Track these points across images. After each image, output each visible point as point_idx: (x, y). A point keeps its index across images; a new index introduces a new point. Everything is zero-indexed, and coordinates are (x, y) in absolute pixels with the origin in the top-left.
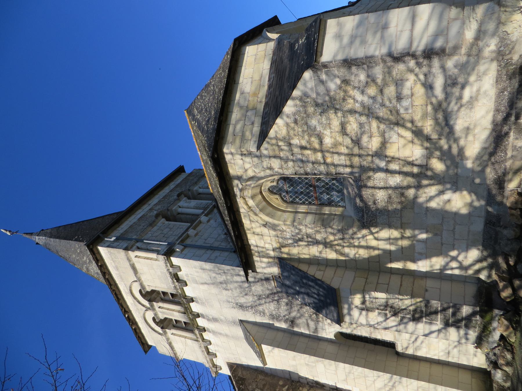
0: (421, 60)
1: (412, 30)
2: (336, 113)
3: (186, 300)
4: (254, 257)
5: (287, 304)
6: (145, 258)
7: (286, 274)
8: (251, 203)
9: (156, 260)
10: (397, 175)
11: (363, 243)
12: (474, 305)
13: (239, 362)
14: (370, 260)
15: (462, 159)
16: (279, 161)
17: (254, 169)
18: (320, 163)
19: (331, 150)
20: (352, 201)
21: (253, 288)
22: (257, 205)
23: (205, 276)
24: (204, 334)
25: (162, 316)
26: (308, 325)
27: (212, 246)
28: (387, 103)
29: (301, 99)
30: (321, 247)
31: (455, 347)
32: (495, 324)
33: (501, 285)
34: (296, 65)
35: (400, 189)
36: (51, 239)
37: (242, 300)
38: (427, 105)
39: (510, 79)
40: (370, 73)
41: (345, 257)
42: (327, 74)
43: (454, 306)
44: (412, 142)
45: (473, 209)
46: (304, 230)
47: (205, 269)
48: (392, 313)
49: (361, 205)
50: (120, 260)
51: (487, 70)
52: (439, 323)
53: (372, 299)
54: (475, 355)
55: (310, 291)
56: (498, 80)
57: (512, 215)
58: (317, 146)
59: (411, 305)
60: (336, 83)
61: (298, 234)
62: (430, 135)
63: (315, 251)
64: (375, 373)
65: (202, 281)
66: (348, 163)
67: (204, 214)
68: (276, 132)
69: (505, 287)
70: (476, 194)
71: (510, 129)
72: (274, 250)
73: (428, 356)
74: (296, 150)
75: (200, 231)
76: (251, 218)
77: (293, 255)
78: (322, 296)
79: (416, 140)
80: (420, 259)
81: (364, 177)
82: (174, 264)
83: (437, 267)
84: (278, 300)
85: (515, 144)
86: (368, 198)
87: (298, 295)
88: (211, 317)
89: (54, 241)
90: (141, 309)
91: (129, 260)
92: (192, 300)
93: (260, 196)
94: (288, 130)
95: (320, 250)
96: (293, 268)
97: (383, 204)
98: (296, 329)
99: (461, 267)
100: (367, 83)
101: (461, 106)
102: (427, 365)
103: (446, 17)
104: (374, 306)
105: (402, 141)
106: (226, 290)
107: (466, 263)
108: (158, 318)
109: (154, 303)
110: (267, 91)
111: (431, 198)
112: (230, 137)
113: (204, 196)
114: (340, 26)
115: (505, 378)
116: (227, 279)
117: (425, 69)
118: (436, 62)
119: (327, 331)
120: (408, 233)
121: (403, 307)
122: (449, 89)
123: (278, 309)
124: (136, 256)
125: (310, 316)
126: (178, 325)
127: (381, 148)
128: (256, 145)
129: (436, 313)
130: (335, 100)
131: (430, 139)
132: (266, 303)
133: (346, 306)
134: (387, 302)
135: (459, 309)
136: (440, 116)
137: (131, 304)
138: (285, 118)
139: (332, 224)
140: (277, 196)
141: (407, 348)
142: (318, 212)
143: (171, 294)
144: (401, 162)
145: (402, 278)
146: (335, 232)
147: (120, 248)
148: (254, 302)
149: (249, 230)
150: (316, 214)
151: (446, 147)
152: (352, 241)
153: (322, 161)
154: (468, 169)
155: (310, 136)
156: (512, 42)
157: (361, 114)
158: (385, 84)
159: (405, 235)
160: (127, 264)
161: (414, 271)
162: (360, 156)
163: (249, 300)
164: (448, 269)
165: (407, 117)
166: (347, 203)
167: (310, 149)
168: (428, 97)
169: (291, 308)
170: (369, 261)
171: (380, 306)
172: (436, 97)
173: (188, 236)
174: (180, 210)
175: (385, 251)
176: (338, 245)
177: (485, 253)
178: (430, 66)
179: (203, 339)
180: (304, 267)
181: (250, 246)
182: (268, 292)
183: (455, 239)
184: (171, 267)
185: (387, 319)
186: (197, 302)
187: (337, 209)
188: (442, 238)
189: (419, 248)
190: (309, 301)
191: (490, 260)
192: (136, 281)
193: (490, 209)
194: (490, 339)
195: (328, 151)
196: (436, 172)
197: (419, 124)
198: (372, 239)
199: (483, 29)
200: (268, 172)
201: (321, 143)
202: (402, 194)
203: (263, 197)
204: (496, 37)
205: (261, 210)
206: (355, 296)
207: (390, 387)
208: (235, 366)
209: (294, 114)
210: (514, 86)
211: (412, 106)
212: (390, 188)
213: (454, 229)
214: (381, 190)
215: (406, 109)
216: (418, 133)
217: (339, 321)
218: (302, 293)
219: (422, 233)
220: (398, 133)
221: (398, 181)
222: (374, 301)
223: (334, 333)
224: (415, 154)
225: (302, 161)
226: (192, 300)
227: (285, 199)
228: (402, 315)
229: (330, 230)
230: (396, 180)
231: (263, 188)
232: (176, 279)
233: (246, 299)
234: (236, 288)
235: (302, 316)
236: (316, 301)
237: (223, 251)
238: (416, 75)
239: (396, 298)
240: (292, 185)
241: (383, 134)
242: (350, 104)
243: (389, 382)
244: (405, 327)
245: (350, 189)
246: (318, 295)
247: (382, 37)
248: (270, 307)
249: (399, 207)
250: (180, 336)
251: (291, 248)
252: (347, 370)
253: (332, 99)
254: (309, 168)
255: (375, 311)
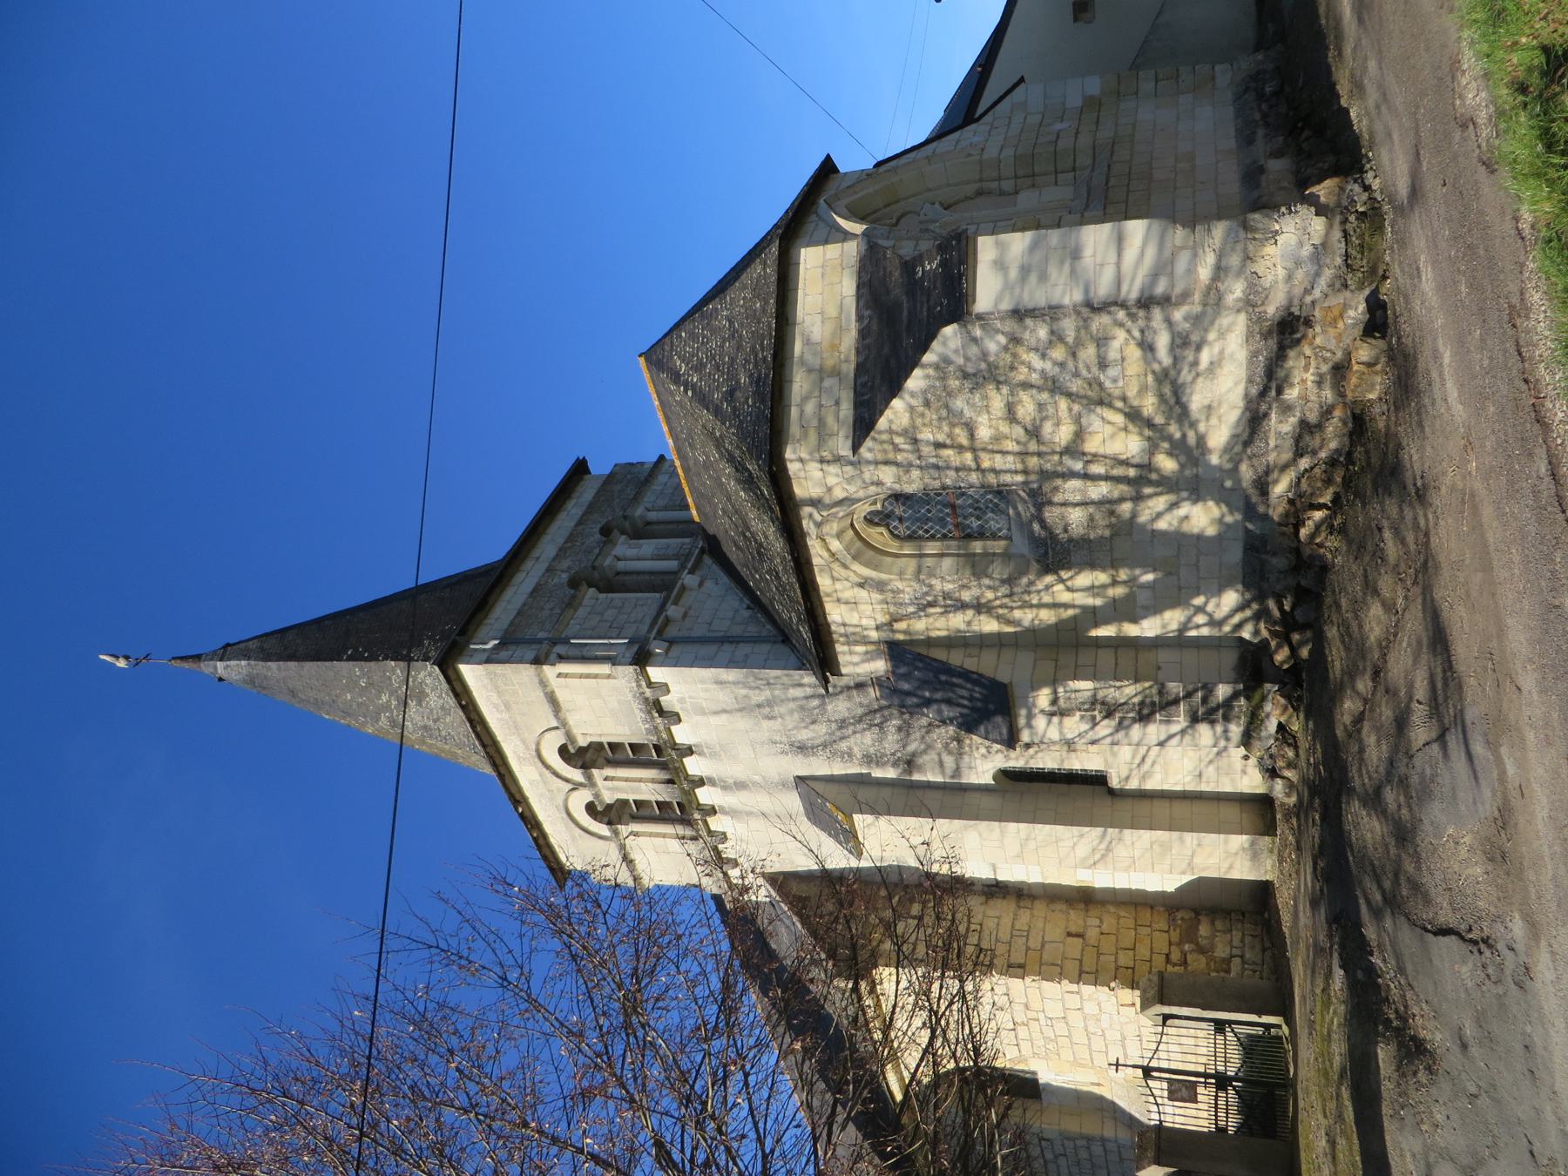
0: (1134, 310)
1: (1118, 265)
2: (998, 389)
3: (679, 752)
4: (837, 646)
5: (900, 729)
6: (581, 676)
7: (902, 670)
8: (835, 545)
9: (609, 677)
10: (1103, 483)
11: (1047, 599)
12: (1235, 682)
13: (788, 868)
14: (1059, 626)
15: (1203, 454)
16: (894, 469)
17: (845, 486)
18: (970, 470)
19: (990, 447)
20: (1025, 526)
21: (829, 707)
22: (847, 549)
23: (724, 697)
24: (710, 820)
25: (609, 798)
26: (941, 764)
27: (728, 634)
28: (1084, 372)
29: (937, 367)
30: (970, 613)
31: (1211, 762)
32: (1268, 707)
33: (1273, 644)
34: (925, 309)
35: (1107, 504)
36: (270, 663)
37: (804, 735)
38: (1146, 375)
39: (1266, 339)
40: (1055, 328)
41: (1015, 627)
42: (983, 327)
43: (1204, 687)
44: (1125, 429)
45: (1226, 530)
46: (936, 583)
47: (725, 683)
48: (1104, 714)
49: (1043, 534)
50: (517, 686)
51: (1233, 323)
52: (1181, 719)
53: (1068, 694)
54: (1244, 772)
55: (953, 696)
56: (1249, 336)
57: (1283, 534)
58: (965, 441)
59: (1136, 695)
60: (998, 343)
61: (926, 594)
62: (1153, 418)
63: (958, 621)
64: (1076, 830)
65: (714, 708)
66: (1019, 467)
67: (686, 571)
68: (891, 421)
69: (1279, 646)
70: (1228, 505)
71: (1270, 408)
72: (878, 628)
73: (1166, 787)
74: (926, 450)
75: (690, 608)
76: (835, 574)
77: (917, 633)
78: (978, 700)
79: (1131, 427)
80: (1145, 617)
81: (1047, 488)
82: (653, 680)
83: (1174, 626)
84: (882, 723)
85: (1279, 430)
86: (1056, 523)
87: (927, 708)
88: (731, 781)
89: (279, 669)
90: (559, 790)
91: (543, 683)
92: (689, 751)
93: (851, 532)
94: (912, 418)
95: (967, 619)
96: (920, 657)
97: (1081, 531)
98: (917, 777)
99: (1213, 623)
100: (1050, 342)
101: (1198, 375)
102: (1166, 803)
103: (1169, 245)
104: (1073, 705)
105: (1109, 429)
106: (770, 718)
107: (1219, 615)
108: (601, 802)
109: (595, 772)
110: (858, 341)
111: (1159, 515)
112: (794, 429)
113: (662, 527)
114: (1001, 247)
115: (1287, 790)
116: (773, 696)
117: (1141, 323)
118: (1157, 313)
119: (980, 769)
120: (1123, 575)
121: (1122, 701)
122: (1178, 351)
123: (881, 742)
124: (559, 675)
125: (946, 746)
126: (644, 812)
127: (1074, 441)
128: (849, 443)
129: (1176, 701)
130: (997, 368)
131: (1153, 425)
132: (855, 732)
133: (1023, 712)
134: (1095, 695)
135: (1211, 691)
136: (1167, 390)
137: (531, 783)
138: (907, 397)
139: (990, 570)
140: (882, 530)
141: (1127, 778)
142: (962, 552)
143: (630, 745)
144: (1107, 461)
145: (1116, 652)
146: (997, 583)
147: (521, 662)
148: (830, 734)
149: (828, 595)
150: (958, 555)
151: (1178, 435)
152: (1027, 598)
153: (973, 465)
154: (1215, 468)
155: (952, 425)
156: (1265, 289)
157: (1040, 389)
158: (1079, 343)
159: (1119, 579)
160: (539, 694)
161: (1137, 638)
162: (1039, 454)
163: (821, 731)
164: (1191, 629)
165: (1117, 392)
166: (1016, 534)
167: (952, 447)
168: (1147, 362)
169: (908, 735)
170: (1057, 630)
171: (1083, 703)
172: (1160, 363)
173: (668, 621)
174: (621, 565)
175: (1085, 609)
176: (1001, 606)
177: (1248, 596)
178: (1148, 319)
179: (710, 832)
180: (939, 654)
181: (828, 625)
182: (860, 711)
183: (1199, 578)
184: (648, 687)
185: (1095, 725)
186: (701, 754)
187: (996, 543)
188: (1179, 579)
189: (1143, 598)
190: (951, 714)
191: (1255, 606)
192: (557, 728)
193: (1250, 526)
194: (1263, 734)
195: (984, 449)
196: (1165, 474)
197: (1136, 403)
198: (1062, 591)
199: (1223, 264)
200: (873, 489)
201: (972, 436)
202: (1112, 513)
203: (857, 533)
204: (1242, 280)
205: (854, 558)
206: (1040, 693)
207: (1102, 852)
208: (781, 878)
209: (924, 392)
210: (1272, 349)
211: (1124, 376)
212: (1093, 503)
213: (1198, 561)
214: (1077, 509)
215: (1115, 381)
216: (1134, 415)
217: (1011, 741)
218: (936, 701)
219: (1145, 573)
220: (1103, 418)
221: (1105, 492)
222: (1073, 696)
223: (992, 772)
224: (1130, 448)
225: (937, 467)
226: (689, 751)
227: (896, 532)
228: (1121, 715)
229: (986, 581)
230: (1099, 491)
231: (855, 517)
232: (657, 712)
233: (813, 731)
234: (791, 712)
235: (929, 747)
236: (965, 711)
237: (755, 642)
238: (1129, 331)
239: (1111, 686)
240: (910, 507)
241: (1077, 420)
242: (1022, 374)
243: (1101, 842)
244: (1127, 735)
245: (1020, 508)
246: (971, 699)
247: (1073, 272)
248: (864, 741)
249: (1107, 533)
250: (651, 835)
251: (912, 621)
252: (1023, 835)
253: (992, 367)
254: (950, 478)
255: (1074, 715)
